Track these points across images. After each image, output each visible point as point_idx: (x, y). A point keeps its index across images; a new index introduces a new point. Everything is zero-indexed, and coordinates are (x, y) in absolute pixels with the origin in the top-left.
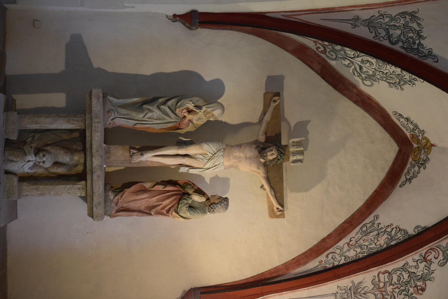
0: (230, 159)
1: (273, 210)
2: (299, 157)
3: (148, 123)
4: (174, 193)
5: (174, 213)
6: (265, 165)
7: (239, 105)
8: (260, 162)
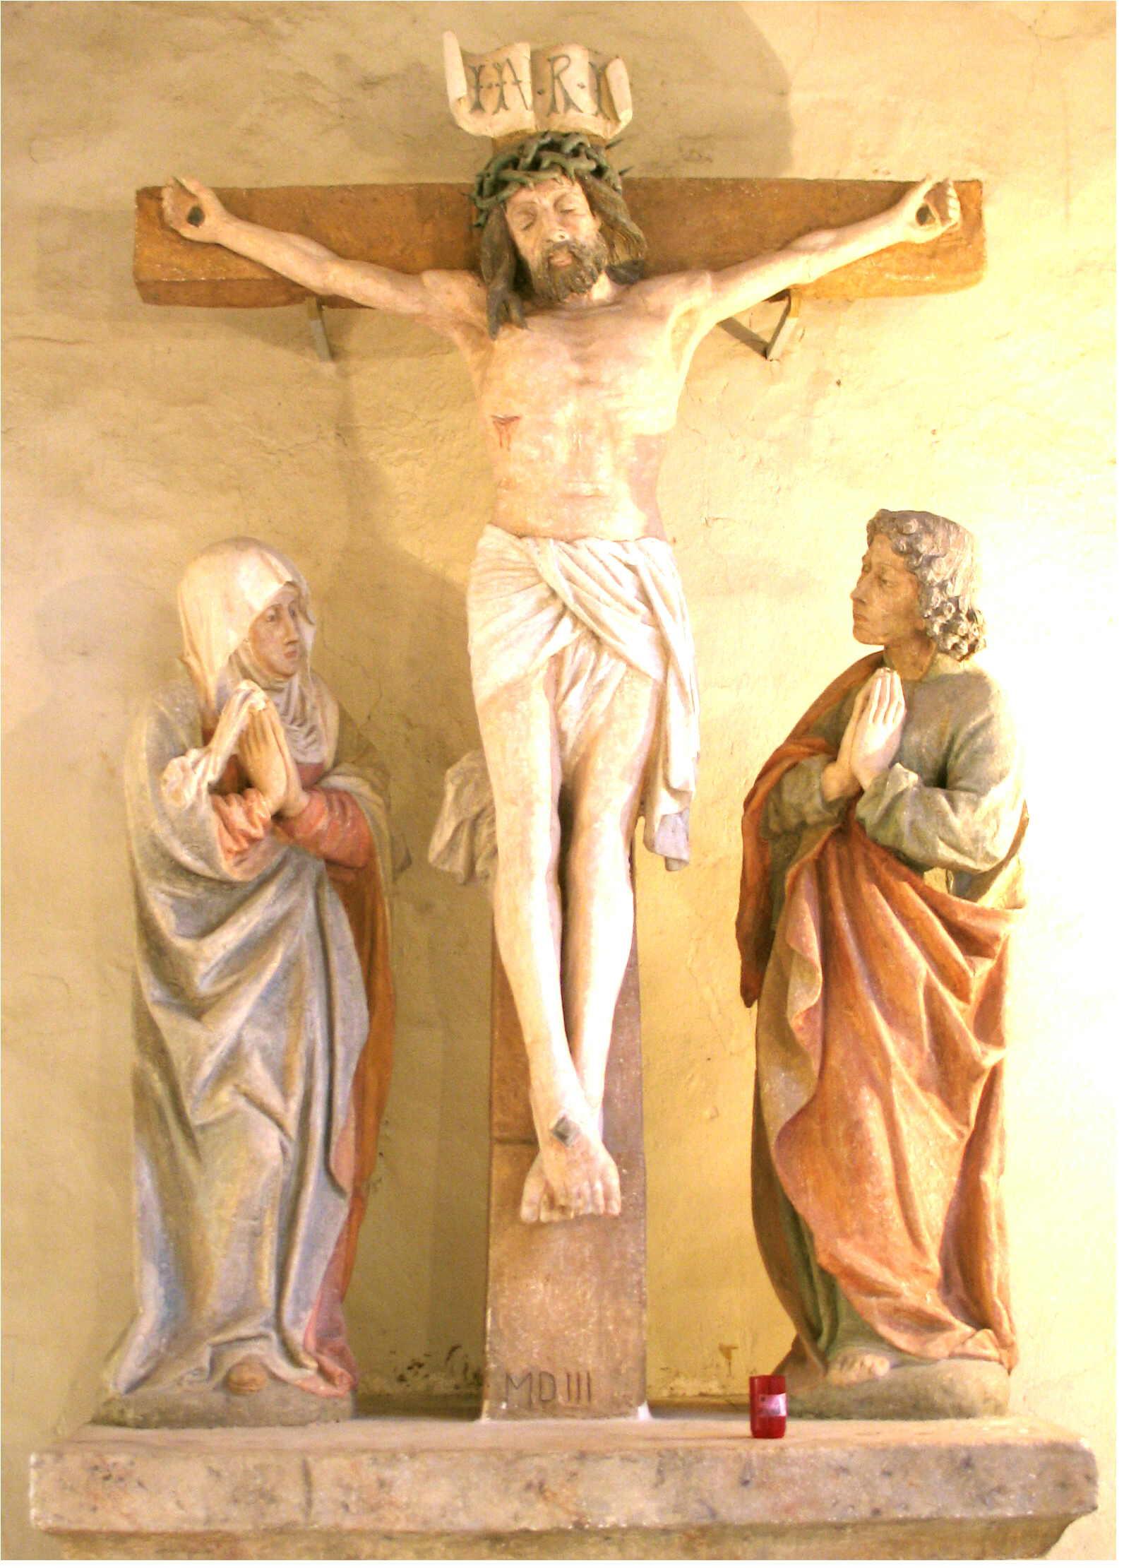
0: (596, 495)
1: (934, 251)
3: (320, 1087)
4: (839, 903)
5: (991, 899)
6: (632, 276)
8: (616, 301)
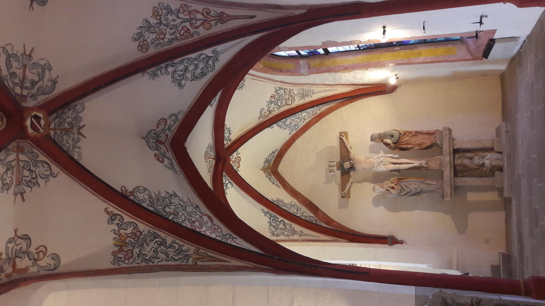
2: (331, 164)
6: (350, 159)
7: (364, 194)
